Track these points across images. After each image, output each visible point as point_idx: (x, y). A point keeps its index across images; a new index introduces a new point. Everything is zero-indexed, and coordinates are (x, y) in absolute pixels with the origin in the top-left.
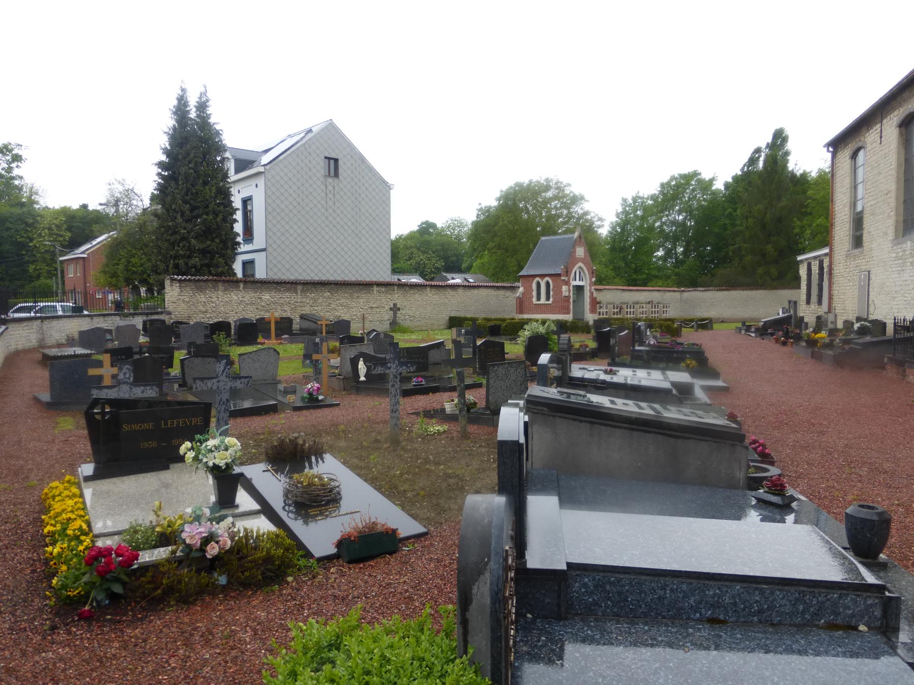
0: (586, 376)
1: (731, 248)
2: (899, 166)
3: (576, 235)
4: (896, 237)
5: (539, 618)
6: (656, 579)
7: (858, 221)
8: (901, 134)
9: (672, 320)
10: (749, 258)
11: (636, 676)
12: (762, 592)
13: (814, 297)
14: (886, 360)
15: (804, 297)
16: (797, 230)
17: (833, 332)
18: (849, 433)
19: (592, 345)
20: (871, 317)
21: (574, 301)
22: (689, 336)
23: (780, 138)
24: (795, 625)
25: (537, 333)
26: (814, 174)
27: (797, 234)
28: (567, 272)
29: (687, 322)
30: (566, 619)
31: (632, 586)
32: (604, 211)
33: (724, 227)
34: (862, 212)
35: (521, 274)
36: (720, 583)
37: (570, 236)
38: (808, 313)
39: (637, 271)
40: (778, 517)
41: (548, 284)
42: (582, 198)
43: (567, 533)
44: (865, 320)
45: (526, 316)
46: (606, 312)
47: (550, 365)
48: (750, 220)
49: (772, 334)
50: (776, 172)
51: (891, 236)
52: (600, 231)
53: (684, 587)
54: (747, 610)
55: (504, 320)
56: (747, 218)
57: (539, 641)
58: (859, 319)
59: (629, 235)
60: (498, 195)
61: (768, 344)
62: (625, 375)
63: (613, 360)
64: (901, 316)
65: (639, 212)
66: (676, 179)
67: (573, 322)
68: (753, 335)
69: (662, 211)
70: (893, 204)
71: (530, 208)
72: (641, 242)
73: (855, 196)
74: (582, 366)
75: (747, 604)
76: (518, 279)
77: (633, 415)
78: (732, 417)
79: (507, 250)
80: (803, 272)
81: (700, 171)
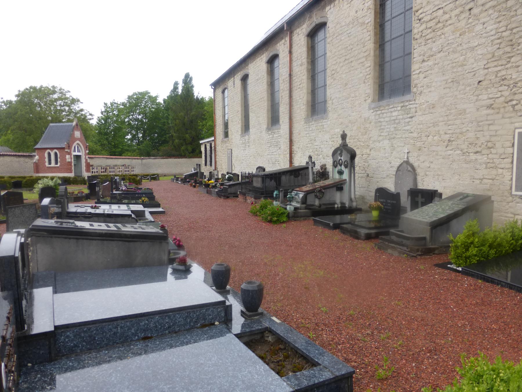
0: (78, 211)
1: (168, 135)
2: (242, 99)
3: (74, 123)
4: (242, 133)
5: (36, 364)
6: (112, 323)
7: (226, 125)
8: (242, 84)
9: (136, 176)
10: (177, 141)
11: (98, 381)
12: (169, 317)
13: (208, 163)
14: (238, 193)
15: (204, 162)
16: (200, 127)
17: (217, 180)
18: (221, 230)
19: (86, 191)
20: (233, 172)
21: (75, 165)
22: (146, 184)
23: (187, 80)
24: (187, 330)
25: (48, 185)
26: (207, 99)
27: (201, 130)
28: (69, 146)
29: (145, 176)
30: (56, 360)
31: (97, 330)
32: (94, 110)
33: (164, 124)
34: (227, 120)
35: (36, 147)
36: (147, 317)
37: (70, 124)
38: (206, 170)
39: (115, 146)
40: (184, 277)
41: (56, 154)
42: (78, 101)
43: (51, 309)
44: (231, 173)
45: (41, 175)
46: (96, 171)
47: (50, 206)
48: (177, 121)
49: (189, 182)
50: (189, 96)
51: (240, 133)
52: (91, 122)
53: (128, 324)
54: (162, 328)
55: (24, 178)
56: (175, 120)
57: (35, 378)
58: (228, 173)
59: (110, 125)
60: (17, 93)
61: (187, 186)
62: (104, 209)
63: (98, 200)
64: (244, 171)
65: (115, 112)
66: (136, 94)
67: (74, 178)
68: (180, 182)
69: (129, 113)
70: (240, 117)
71: (42, 105)
72: (117, 130)
73: (225, 112)
74: (77, 205)
75: (162, 325)
76: (35, 150)
77: (104, 232)
78: (163, 228)
79: (26, 131)
80: (203, 149)
81: (149, 91)
